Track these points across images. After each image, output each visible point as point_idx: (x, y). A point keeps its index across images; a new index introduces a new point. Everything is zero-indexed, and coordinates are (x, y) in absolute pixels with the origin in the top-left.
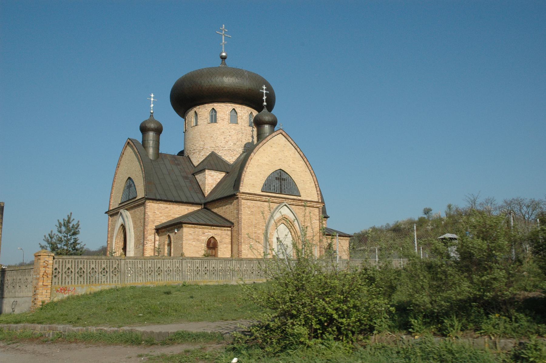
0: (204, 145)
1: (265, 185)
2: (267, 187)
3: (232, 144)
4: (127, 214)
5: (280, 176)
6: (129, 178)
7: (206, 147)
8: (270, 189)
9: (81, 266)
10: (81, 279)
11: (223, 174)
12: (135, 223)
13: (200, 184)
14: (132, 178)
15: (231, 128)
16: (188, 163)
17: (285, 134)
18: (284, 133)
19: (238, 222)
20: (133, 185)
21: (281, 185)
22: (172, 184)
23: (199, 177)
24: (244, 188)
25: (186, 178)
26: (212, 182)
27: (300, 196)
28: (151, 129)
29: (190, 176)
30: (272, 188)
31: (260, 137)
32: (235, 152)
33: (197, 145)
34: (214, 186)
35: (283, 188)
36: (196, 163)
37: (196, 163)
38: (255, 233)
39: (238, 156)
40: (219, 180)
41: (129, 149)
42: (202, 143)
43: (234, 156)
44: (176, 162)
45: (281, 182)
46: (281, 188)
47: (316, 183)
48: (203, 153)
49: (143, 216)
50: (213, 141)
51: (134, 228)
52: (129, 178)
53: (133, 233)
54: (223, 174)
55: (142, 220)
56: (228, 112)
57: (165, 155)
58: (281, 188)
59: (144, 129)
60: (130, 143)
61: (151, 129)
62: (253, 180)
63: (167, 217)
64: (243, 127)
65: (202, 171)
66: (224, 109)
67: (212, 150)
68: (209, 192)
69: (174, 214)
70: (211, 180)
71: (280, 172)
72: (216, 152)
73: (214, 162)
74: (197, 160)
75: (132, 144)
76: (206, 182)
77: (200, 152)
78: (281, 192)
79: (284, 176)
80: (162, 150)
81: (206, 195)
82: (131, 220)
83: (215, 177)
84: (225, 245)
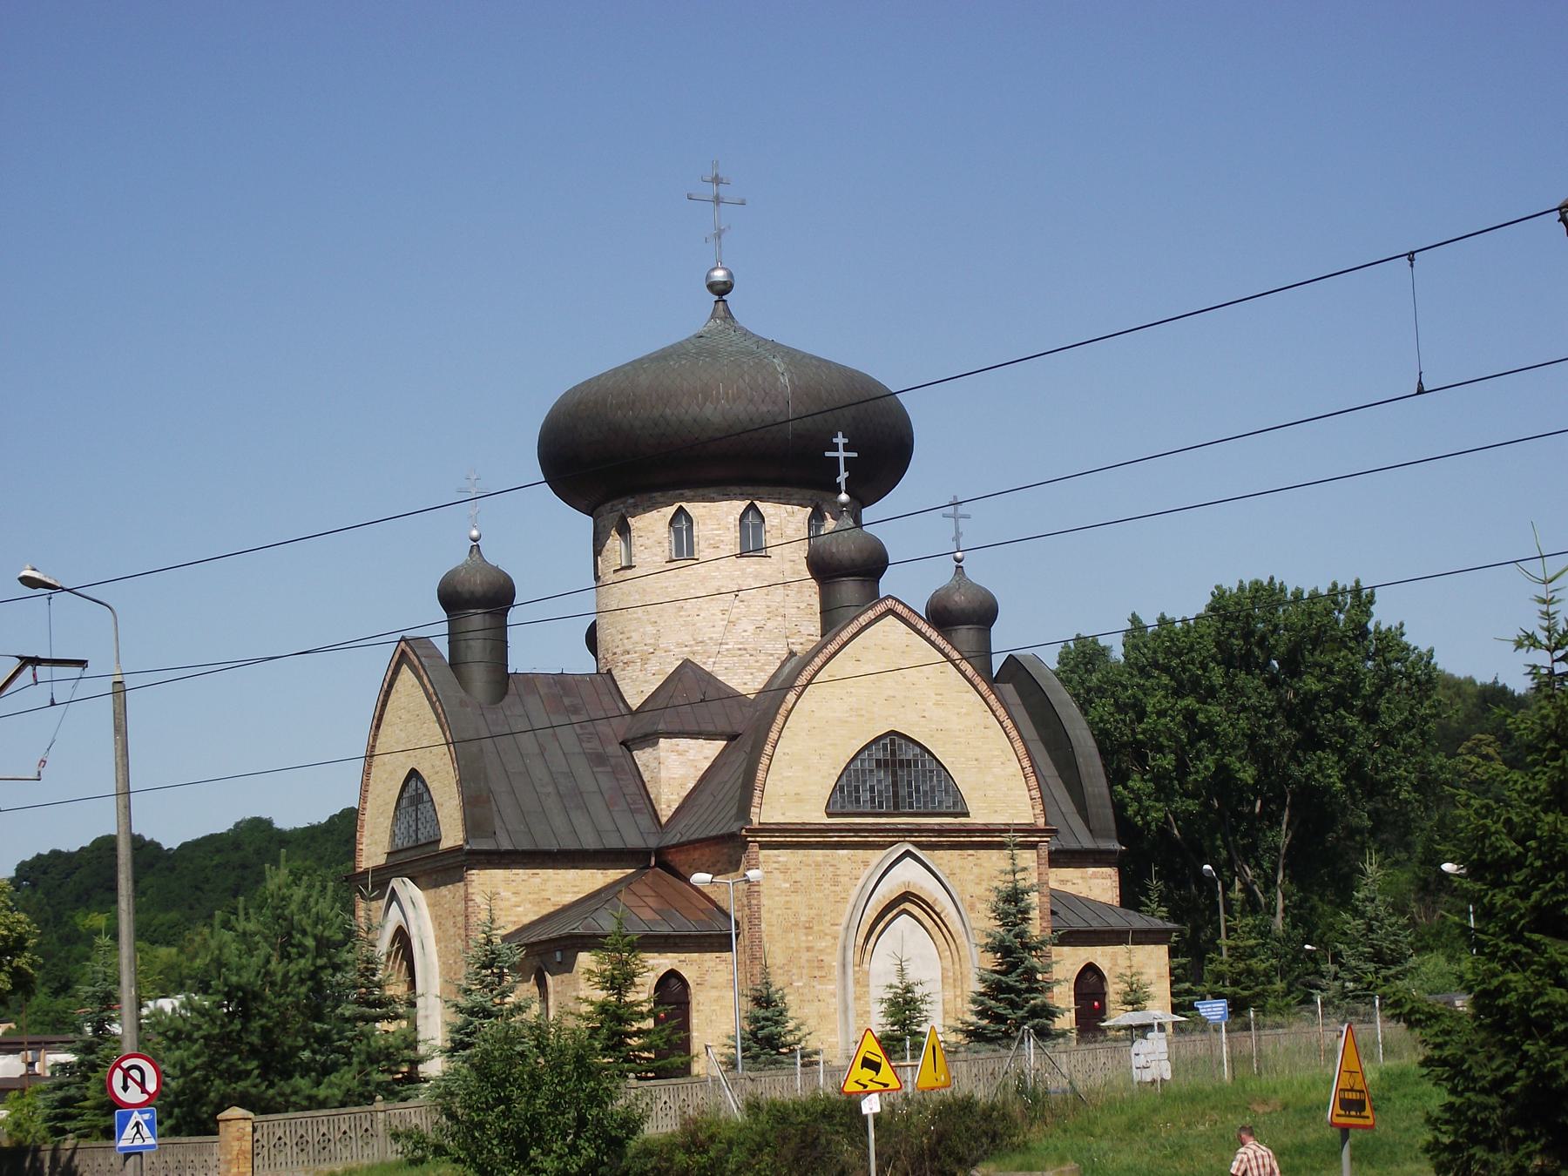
0: (658, 636)
1: (838, 788)
2: (846, 793)
3: (751, 628)
4: (406, 889)
5: (893, 753)
6: (414, 774)
7: (663, 643)
8: (858, 800)
9: (301, 1131)
10: (303, 1157)
11: (720, 744)
12: (438, 921)
13: (646, 777)
14: (424, 774)
15: (743, 570)
16: (606, 699)
17: (905, 613)
18: (899, 609)
19: (754, 919)
20: (426, 797)
21: (895, 784)
22: (550, 789)
23: (642, 757)
24: (771, 808)
25: (599, 759)
26: (682, 772)
27: (967, 815)
28: (479, 601)
29: (614, 749)
30: (865, 796)
31: (831, 618)
32: (762, 658)
33: (636, 636)
34: (691, 785)
35: (903, 792)
36: (635, 702)
37: (635, 702)
38: (809, 949)
39: (772, 670)
40: (707, 765)
41: (406, 674)
42: (650, 629)
43: (761, 669)
44: (567, 701)
45: (894, 774)
46: (896, 794)
47: (1026, 763)
48: (653, 666)
49: (461, 906)
50: (686, 624)
51: (438, 941)
52: (414, 774)
53: (435, 958)
54: (720, 744)
55: (461, 920)
56: (731, 519)
57: (530, 680)
58: (896, 794)
59: (453, 599)
60: (409, 654)
61: (479, 601)
62: (796, 783)
63: (537, 903)
64: (788, 566)
65: (649, 739)
66: (716, 519)
67: (685, 653)
68: (675, 806)
69: (560, 892)
70: (676, 767)
71: (893, 742)
72: (697, 660)
73: (691, 701)
74: (637, 687)
75: (416, 662)
76: (663, 774)
77: (645, 661)
78: (896, 806)
79: (910, 753)
80: (517, 662)
81: (664, 820)
82: (425, 911)
83: (691, 755)
84: (714, 994)
